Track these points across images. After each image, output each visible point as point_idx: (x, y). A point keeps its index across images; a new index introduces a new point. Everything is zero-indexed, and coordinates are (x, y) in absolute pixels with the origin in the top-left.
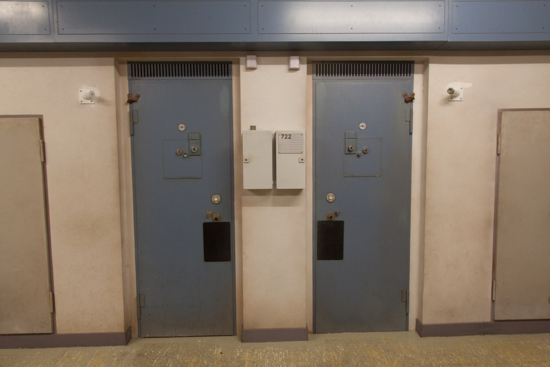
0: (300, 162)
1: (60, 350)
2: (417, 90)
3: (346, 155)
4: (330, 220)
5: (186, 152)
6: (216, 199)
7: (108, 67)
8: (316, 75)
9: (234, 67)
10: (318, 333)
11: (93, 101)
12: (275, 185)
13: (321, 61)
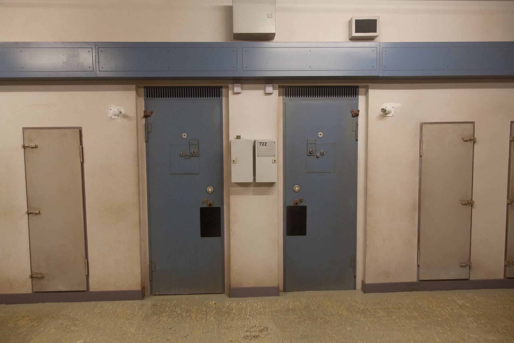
0: (273, 163)
1: (93, 303)
2: (361, 107)
3: (308, 156)
4: (296, 205)
5: (188, 154)
6: (210, 190)
7: (131, 92)
8: (285, 96)
9: (224, 90)
10: (287, 292)
11: (119, 117)
12: (254, 179)
13: (289, 86)
